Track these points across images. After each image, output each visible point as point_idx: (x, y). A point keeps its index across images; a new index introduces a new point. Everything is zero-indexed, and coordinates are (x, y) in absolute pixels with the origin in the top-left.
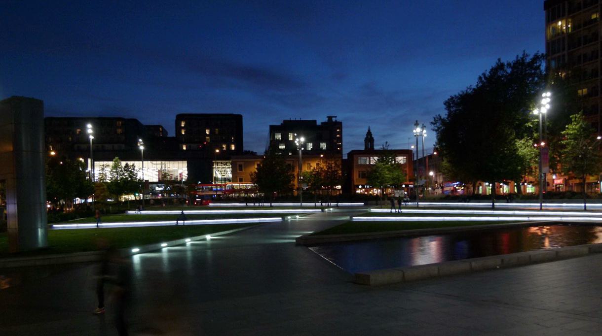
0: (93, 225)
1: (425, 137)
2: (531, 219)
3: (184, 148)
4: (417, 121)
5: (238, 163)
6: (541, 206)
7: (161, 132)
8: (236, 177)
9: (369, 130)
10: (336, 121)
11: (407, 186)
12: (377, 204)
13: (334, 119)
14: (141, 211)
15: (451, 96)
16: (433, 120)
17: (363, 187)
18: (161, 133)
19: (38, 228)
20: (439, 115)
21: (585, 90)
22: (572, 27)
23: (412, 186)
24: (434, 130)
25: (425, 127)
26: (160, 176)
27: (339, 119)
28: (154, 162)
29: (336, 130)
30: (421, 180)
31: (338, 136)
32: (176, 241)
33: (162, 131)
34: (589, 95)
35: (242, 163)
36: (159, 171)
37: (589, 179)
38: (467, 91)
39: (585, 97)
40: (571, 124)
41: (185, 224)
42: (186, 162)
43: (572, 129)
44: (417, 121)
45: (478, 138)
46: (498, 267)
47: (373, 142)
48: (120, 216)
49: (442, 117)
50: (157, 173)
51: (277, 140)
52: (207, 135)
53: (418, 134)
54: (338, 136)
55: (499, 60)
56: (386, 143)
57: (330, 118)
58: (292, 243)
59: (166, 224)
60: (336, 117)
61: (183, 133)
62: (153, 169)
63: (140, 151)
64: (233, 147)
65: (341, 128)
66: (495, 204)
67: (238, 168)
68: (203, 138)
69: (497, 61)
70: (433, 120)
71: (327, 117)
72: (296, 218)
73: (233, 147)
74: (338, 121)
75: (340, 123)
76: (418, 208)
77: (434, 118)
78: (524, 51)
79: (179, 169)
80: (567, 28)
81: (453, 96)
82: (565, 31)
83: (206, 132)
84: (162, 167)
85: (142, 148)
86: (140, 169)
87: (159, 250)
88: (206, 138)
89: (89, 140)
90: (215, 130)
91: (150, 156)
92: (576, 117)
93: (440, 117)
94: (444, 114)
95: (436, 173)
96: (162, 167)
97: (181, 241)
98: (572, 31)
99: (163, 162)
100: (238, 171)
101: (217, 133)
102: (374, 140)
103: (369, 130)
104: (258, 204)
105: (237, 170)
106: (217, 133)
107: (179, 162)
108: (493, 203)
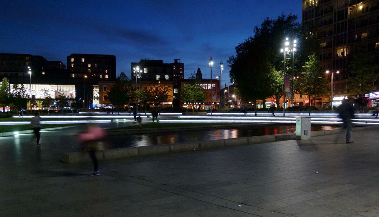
2: (273, 121)
6: (284, 115)
7: (61, 66)
10: (180, 62)
11: (215, 103)
13: (178, 61)
14: (22, 115)
16: (229, 60)
18: (61, 67)
21: (325, 44)
22: (318, 3)
23: (219, 103)
28: (53, 85)
31: (181, 72)
32: (3, 133)
34: (327, 47)
35: (106, 86)
36: (56, 92)
37: (324, 100)
38: (248, 39)
39: (324, 48)
40: (309, 61)
42: (74, 86)
43: (309, 64)
44: (211, 57)
45: (253, 72)
46: (194, 150)
49: (235, 58)
50: (55, 93)
52: (89, 68)
53: (212, 66)
55: (268, 18)
57: (176, 60)
59: (26, 123)
60: (180, 60)
61: (73, 66)
63: (29, 75)
64: (101, 76)
65: (183, 67)
66: (257, 114)
67: (103, 89)
68: (91, 72)
69: (266, 19)
70: (229, 60)
71: (174, 60)
73: (107, 77)
74: (181, 62)
77: (230, 58)
78: (283, 13)
79: (70, 91)
80: (315, 3)
81: (241, 43)
82: (314, 5)
83: (88, 66)
84: (58, 89)
86: (42, 90)
90: (95, 65)
91: (38, 80)
92: (311, 57)
93: (234, 57)
94: (235, 54)
96: (58, 89)
97: (9, 133)
98: (318, 5)
100: (103, 91)
101: (96, 66)
103: (199, 69)
104: (112, 113)
105: (102, 90)
106: (96, 66)
107: (70, 85)
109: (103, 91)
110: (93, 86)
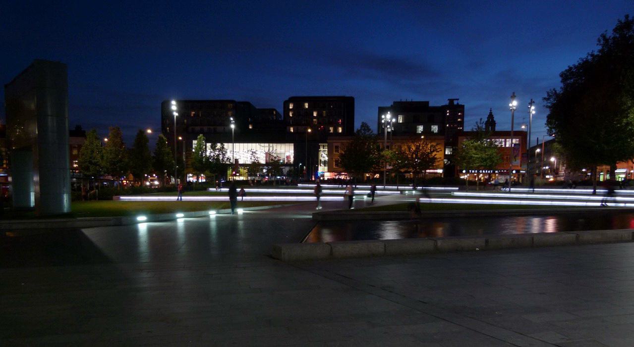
0: (184, 198)
1: (533, 115)
3: (292, 130)
4: (514, 93)
5: (335, 144)
8: (332, 159)
9: (491, 116)
10: (458, 103)
11: (518, 171)
12: (485, 190)
13: (455, 102)
14: (221, 188)
15: (569, 67)
16: (546, 96)
17: (467, 172)
19: (31, 192)
20: (554, 89)
24: (547, 107)
25: (534, 102)
26: (268, 159)
27: (461, 102)
28: (263, 144)
29: (457, 114)
30: (516, 161)
31: (459, 120)
33: (276, 115)
35: (339, 144)
36: (266, 154)
41: (244, 200)
44: (514, 93)
47: (495, 126)
48: (204, 192)
49: (558, 92)
50: (265, 155)
51: (622, 181)
53: (514, 108)
54: (459, 120)
56: (481, 119)
57: (451, 101)
58: (309, 219)
60: (458, 100)
61: (291, 116)
62: (261, 151)
64: (331, 129)
65: (463, 112)
66: (597, 191)
70: (546, 96)
72: (363, 198)
74: (460, 104)
75: (463, 107)
76: (510, 192)
77: (548, 93)
79: (286, 152)
81: (571, 66)
84: (269, 150)
85: (233, 126)
86: (248, 151)
87: (174, 220)
88: (313, 121)
89: (173, 116)
91: (243, 137)
93: (556, 91)
95: (558, 159)
97: (203, 213)
99: (271, 145)
100: (334, 153)
101: (324, 115)
102: (495, 124)
106: (324, 115)
108: (595, 189)
109: (334, 153)
110: (320, 144)
